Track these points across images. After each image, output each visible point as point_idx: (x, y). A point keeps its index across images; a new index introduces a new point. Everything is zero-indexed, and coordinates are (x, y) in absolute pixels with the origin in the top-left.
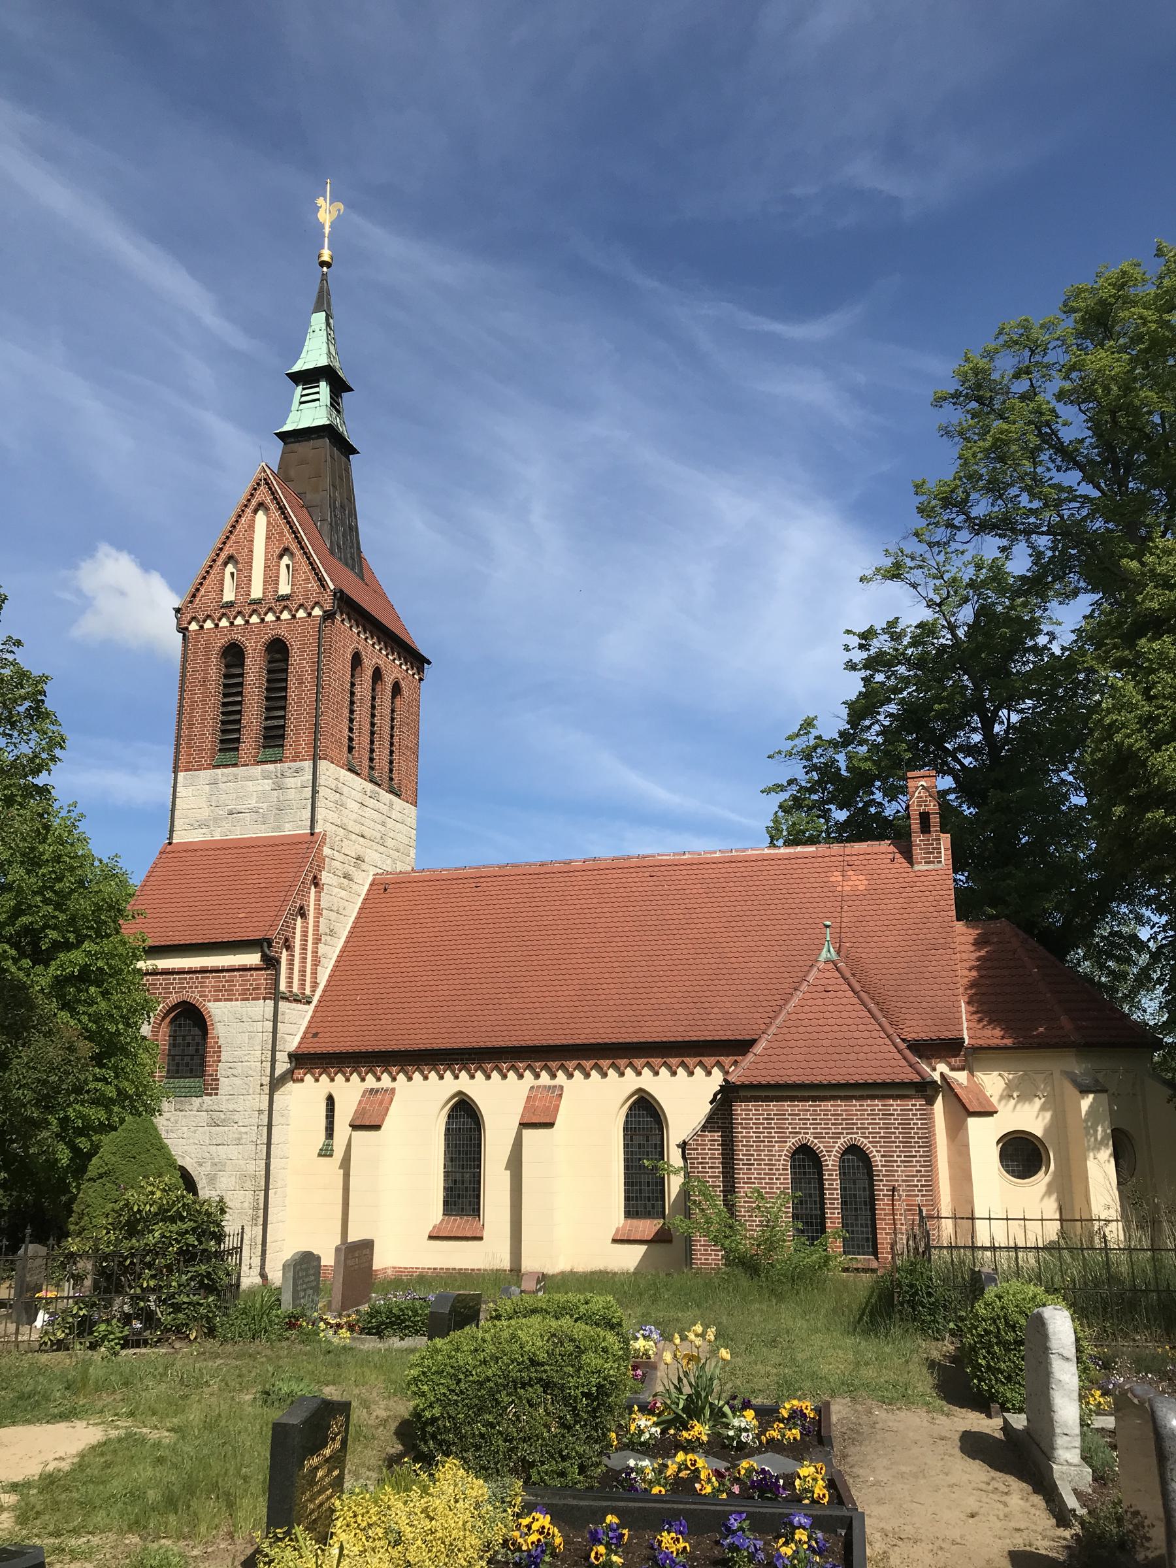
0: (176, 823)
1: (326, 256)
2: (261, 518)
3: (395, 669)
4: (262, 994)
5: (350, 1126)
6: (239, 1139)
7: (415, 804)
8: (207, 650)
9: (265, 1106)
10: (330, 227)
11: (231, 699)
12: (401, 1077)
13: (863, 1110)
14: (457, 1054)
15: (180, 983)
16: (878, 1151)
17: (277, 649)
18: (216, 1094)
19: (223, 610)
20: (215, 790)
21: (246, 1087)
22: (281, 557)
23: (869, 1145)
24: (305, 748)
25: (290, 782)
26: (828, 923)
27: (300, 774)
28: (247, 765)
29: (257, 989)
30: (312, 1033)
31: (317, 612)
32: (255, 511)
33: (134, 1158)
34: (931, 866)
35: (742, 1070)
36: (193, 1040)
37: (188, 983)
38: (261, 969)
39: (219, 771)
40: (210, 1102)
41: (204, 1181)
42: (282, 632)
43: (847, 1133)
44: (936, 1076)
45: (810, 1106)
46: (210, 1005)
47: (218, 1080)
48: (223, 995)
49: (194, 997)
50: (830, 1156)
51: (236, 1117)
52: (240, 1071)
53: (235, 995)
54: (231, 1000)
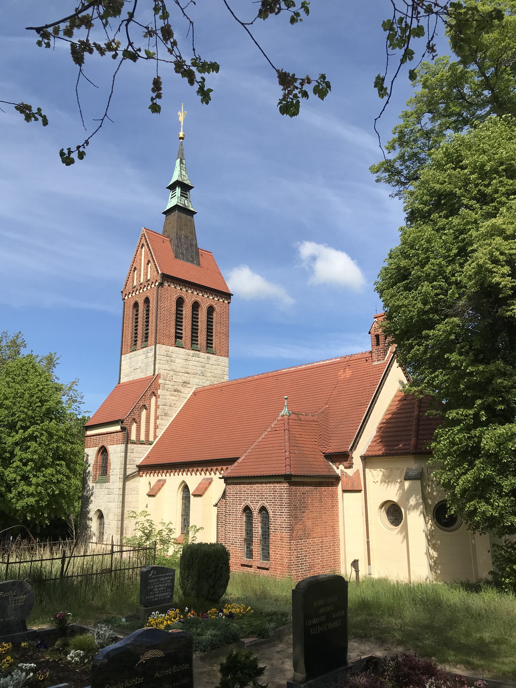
5: (147, 495)
6: (114, 500)
7: (228, 356)
13: (266, 488)
14: (182, 465)
16: (271, 510)
17: (147, 301)
23: (268, 506)
26: (286, 397)
34: (379, 362)
35: (231, 470)
38: (120, 432)
43: (261, 501)
44: (338, 472)
45: (250, 487)
46: (109, 447)
50: (255, 511)
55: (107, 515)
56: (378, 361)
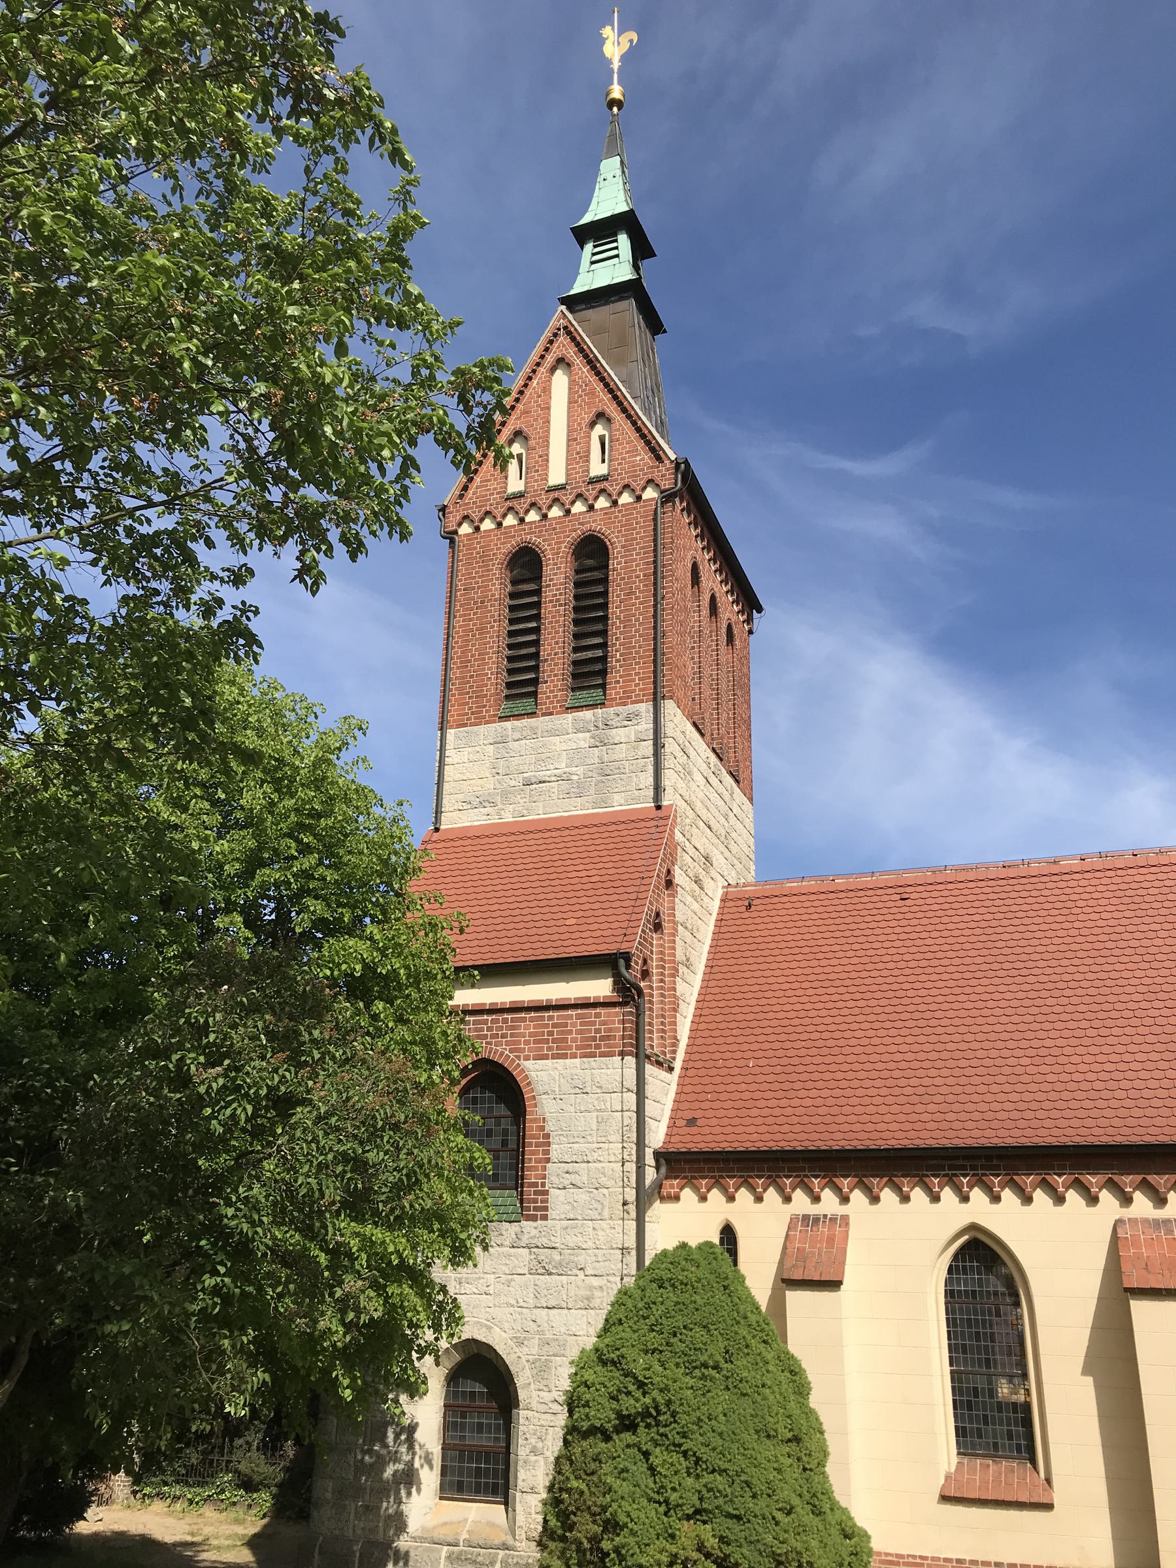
0: (445, 801)
1: (617, 92)
2: (560, 381)
3: (730, 610)
4: (616, 1046)
8: (485, 558)
9: (631, 1242)
10: (620, 61)
11: (521, 626)
12: (858, 1197)
15: (476, 1030)
18: (545, 1218)
19: (509, 504)
20: (503, 751)
21: (596, 1205)
22: (592, 424)
24: (640, 680)
25: (619, 734)
27: (635, 721)
28: (551, 714)
29: (608, 1038)
30: (683, 1119)
31: (650, 494)
32: (553, 370)
33: (716, 1367)
36: (498, 1124)
37: (489, 1029)
39: (508, 725)
40: (534, 1232)
41: (528, 1373)
42: (596, 525)
46: (529, 1064)
47: (546, 1193)
48: (549, 1049)
49: (500, 1052)
51: (581, 1258)
52: (585, 1179)
53: (570, 1048)
54: (564, 1056)
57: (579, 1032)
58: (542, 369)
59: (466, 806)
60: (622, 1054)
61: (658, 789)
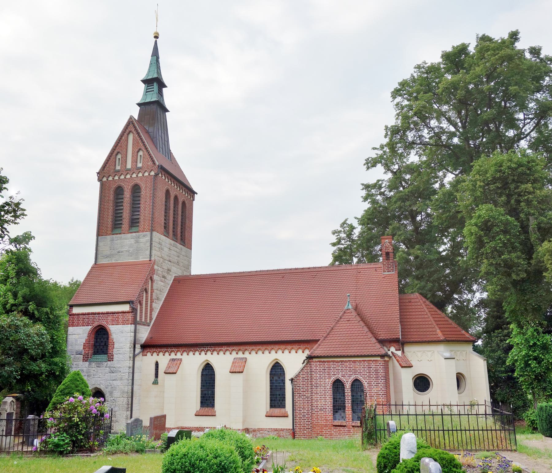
16: (366, 381)
18: (113, 361)
34: (390, 273)
47: (113, 355)
49: (104, 323)
54: (118, 324)
55: (111, 393)
56: (388, 271)
57: (122, 319)
58: (125, 134)
59: (103, 258)
60: (131, 324)
61: (151, 255)
